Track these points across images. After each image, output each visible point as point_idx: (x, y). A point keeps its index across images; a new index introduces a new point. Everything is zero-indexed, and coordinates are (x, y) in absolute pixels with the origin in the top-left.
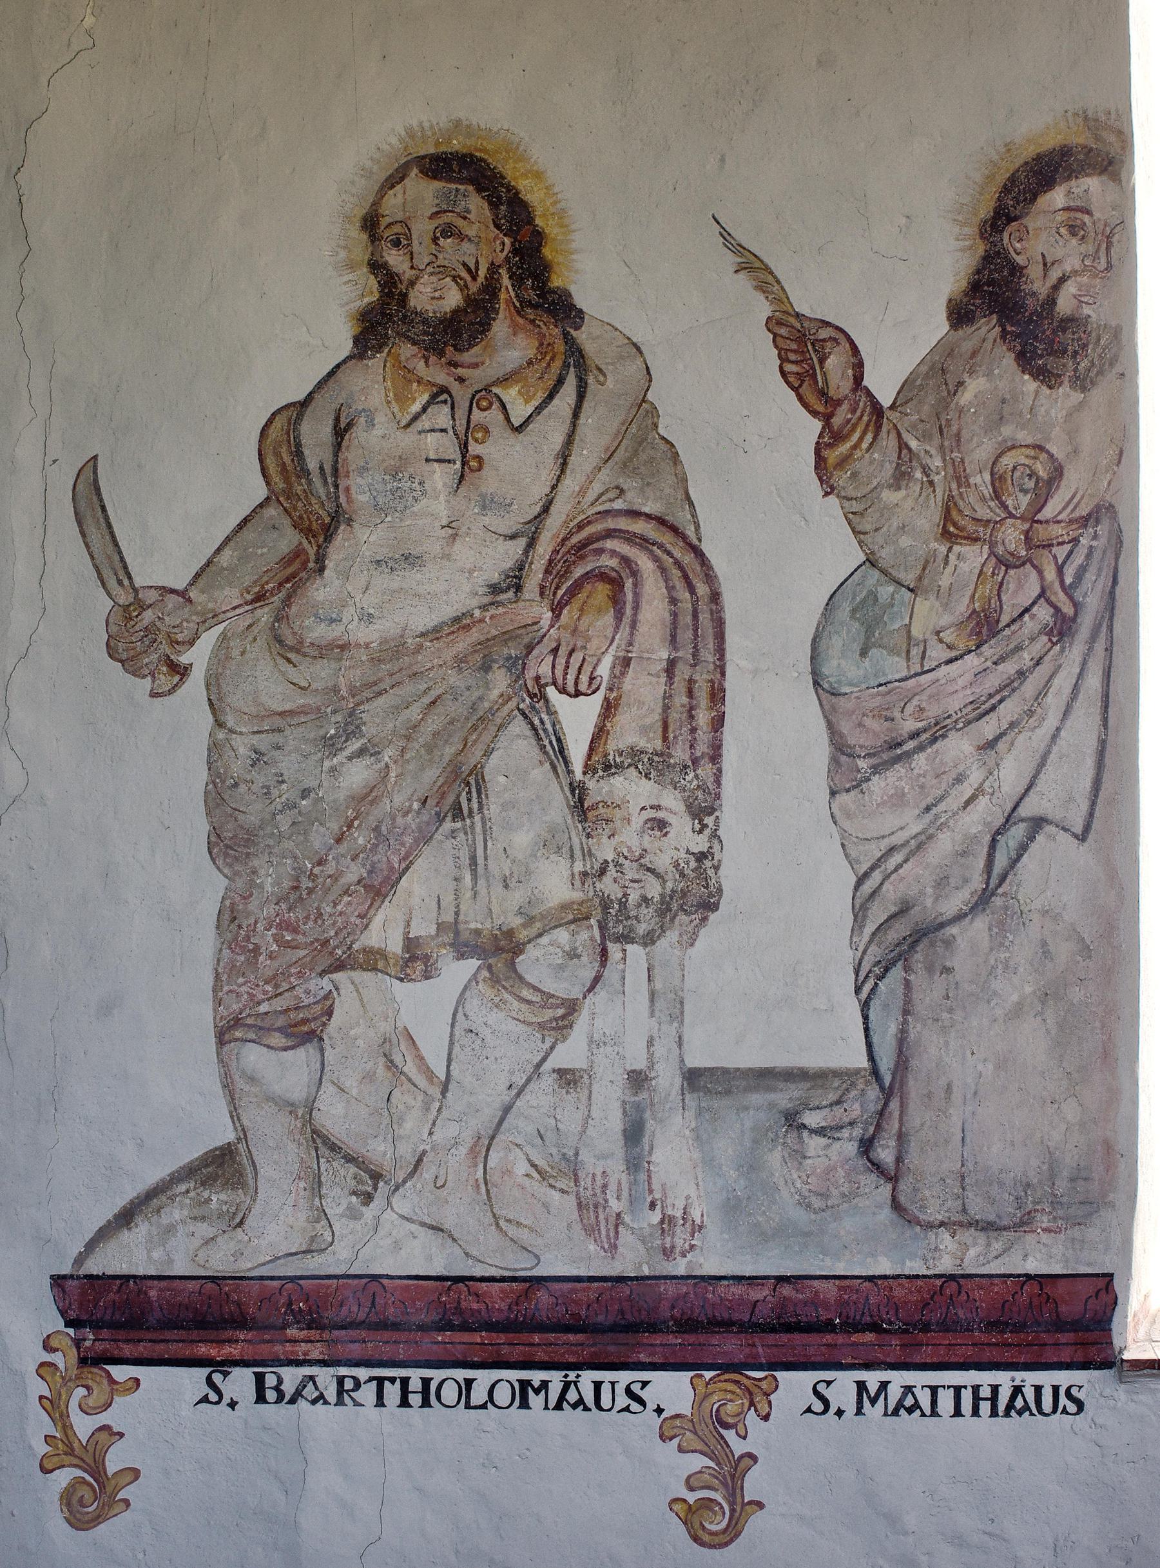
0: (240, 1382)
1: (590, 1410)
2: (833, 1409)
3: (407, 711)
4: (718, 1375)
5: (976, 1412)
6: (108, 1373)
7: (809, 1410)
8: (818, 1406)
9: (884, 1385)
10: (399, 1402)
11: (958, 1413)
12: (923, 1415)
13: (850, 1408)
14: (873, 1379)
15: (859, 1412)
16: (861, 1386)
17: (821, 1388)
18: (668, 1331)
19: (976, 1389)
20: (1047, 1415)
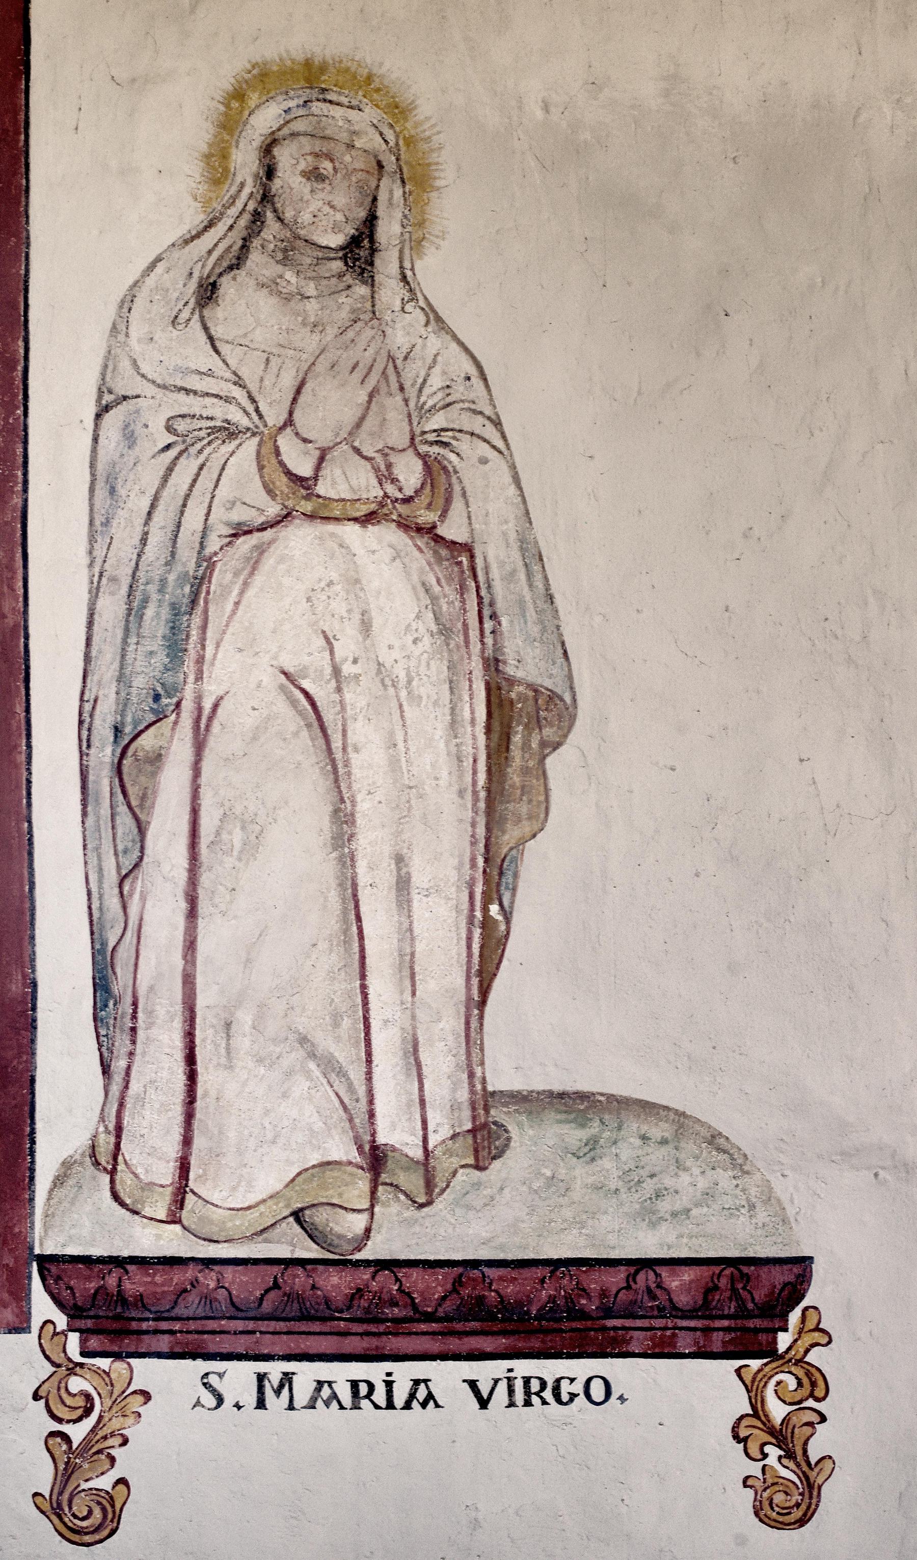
0: (238, 1378)
1: (548, 1404)
2: (228, 1403)
3: (481, 870)
4: (766, 1365)
5: (528, 1403)
6: (129, 1364)
7: (198, 1403)
8: (209, 1400)
9: (287, 1378)
10: (255, 1405)
11: (512, 1404)
12: (342, 1407)
13: (250, 1399)
14: (275, 1370)
15: (261, 1404)
16: (261, 1378)
17: (213, 1380)
18: (756, 1317)
19: (527, 1381)
20: (566, 1404)
